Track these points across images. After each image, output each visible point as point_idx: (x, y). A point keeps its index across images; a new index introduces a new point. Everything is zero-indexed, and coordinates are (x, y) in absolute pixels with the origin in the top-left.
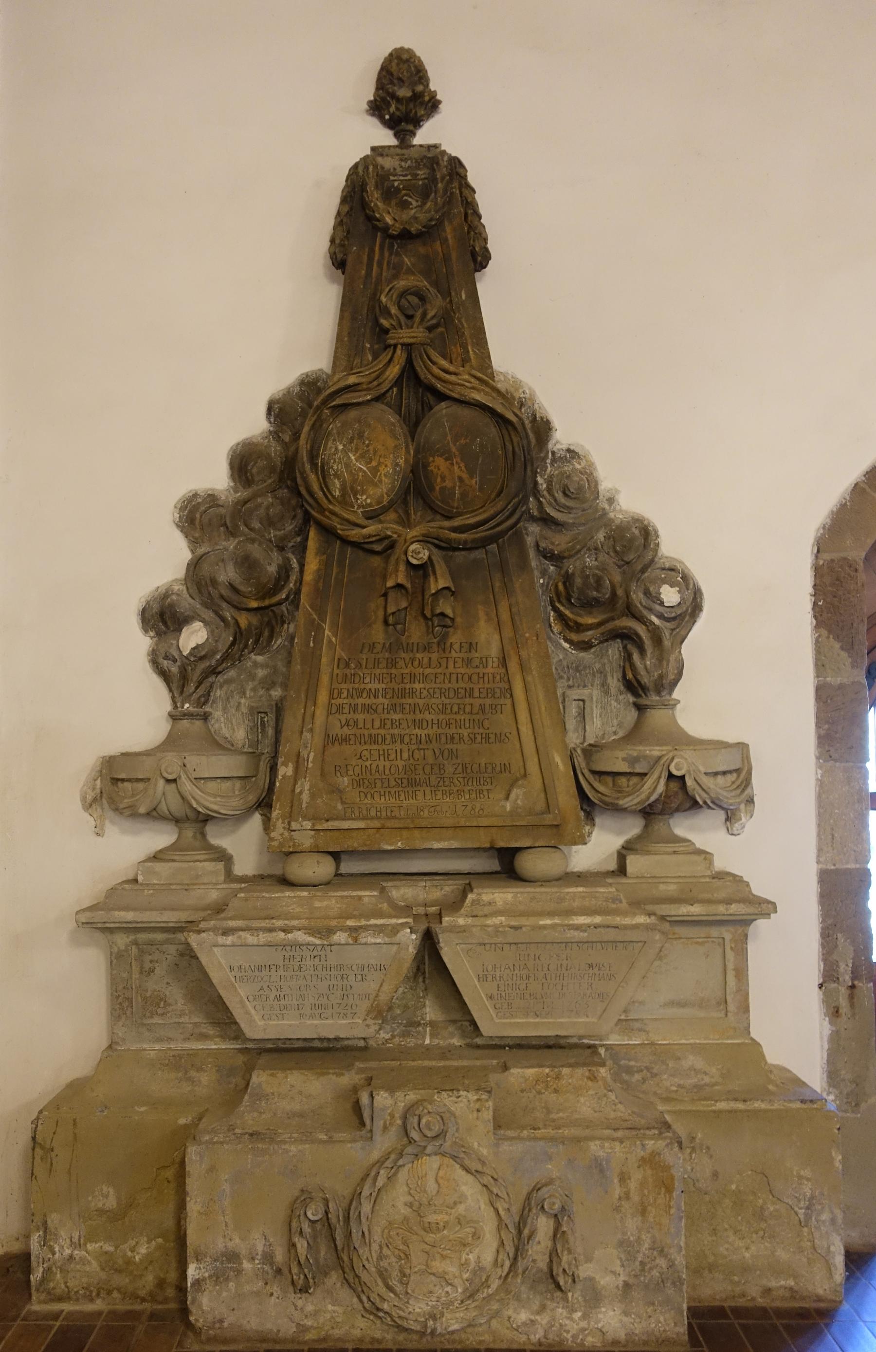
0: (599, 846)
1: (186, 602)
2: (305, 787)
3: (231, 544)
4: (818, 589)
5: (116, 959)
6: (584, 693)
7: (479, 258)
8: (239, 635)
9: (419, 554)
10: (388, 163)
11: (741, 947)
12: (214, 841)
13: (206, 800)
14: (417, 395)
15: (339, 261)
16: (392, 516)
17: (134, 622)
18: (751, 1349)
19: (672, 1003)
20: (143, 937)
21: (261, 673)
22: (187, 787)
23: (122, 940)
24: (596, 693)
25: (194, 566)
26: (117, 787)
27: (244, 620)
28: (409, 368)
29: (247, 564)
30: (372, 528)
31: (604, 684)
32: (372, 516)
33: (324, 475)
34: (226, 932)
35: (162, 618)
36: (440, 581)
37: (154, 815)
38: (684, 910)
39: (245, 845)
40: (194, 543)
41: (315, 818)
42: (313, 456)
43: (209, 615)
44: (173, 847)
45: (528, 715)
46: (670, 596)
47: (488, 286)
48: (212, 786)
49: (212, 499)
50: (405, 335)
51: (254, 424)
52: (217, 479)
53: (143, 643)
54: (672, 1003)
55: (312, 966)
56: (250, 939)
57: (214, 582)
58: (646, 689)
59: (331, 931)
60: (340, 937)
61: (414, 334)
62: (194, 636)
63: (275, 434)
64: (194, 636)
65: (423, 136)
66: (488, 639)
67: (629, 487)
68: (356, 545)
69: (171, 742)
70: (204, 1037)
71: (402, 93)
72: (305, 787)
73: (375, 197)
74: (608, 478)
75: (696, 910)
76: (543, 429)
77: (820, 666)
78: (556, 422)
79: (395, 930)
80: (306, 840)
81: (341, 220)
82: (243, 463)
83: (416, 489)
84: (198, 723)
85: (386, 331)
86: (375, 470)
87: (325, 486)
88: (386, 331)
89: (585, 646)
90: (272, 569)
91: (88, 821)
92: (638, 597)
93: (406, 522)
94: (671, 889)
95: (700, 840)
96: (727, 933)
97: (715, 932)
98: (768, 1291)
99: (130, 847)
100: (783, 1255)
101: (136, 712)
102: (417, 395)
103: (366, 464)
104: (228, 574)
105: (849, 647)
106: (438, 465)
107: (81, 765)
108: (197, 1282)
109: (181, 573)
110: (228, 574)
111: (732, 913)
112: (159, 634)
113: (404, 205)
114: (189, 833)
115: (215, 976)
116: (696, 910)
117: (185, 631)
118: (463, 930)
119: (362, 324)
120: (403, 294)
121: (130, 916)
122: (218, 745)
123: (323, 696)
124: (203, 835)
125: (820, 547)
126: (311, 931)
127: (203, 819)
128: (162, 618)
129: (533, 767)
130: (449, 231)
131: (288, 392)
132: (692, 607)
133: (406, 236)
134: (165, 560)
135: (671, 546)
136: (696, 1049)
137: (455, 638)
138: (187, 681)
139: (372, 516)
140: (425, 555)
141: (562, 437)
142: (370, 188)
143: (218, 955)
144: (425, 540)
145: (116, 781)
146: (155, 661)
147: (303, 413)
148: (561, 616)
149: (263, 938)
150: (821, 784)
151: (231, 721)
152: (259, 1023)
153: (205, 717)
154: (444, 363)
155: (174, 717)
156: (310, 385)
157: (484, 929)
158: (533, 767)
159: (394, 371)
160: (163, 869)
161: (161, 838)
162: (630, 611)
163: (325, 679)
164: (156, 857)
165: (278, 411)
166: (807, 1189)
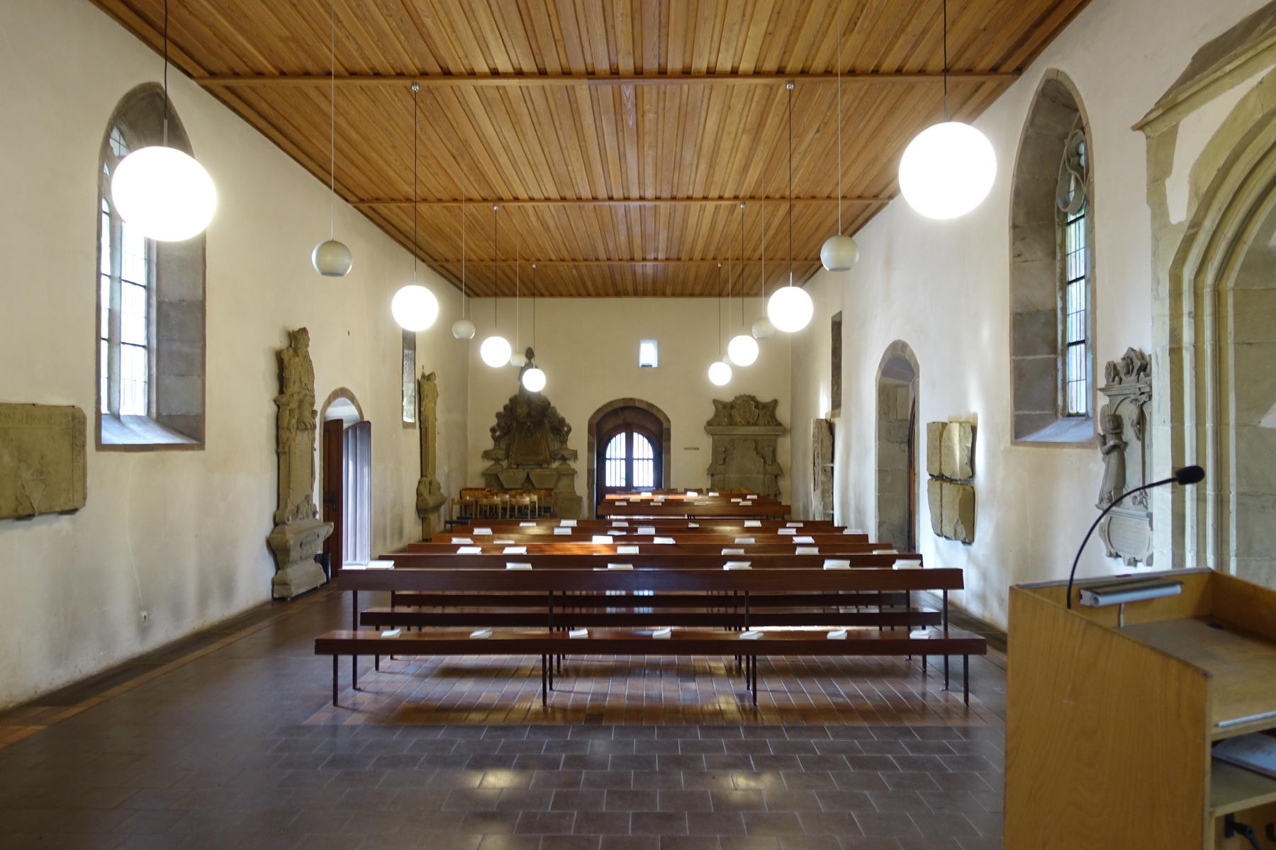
0: (555, 465)
4: (1166, 209)
18: (205, 3)
26: (486, 455)
35: (493, 430)
39: (505, 464)
45: (1250, 181)
52: (501, 410)
53: (490, 434)
58: (564, 442)
62: (498, 434)
64: (498, 434)
82: (505, 408)
99: (488, 464)
101: (489, 444)
107: (482, 451)
111: (573, 473)
132: (570, 430)
134: (494, 422)
135: (567, 421)
138: (496, 440)
143: (501, 477)
151: (503, 446)
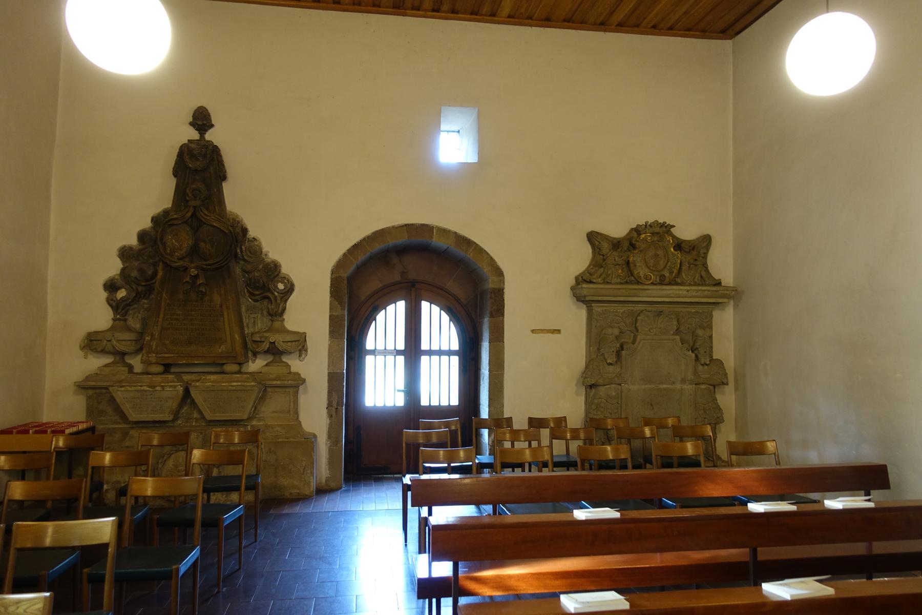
1: (120, 282)
2: (154, 344)
3: (136, 264)
5: (89, 398)
6: (255, 316)
7: (224, 178)
8: (138, 293)
9: (193, 272)
10: (193, 146)
11: (296, 394)
12: (128, 361)
13: (121, 347)
14: (196, 223)
15: (175, 174)
16: (187, 259)
17: (101, 289)
19: (274, 412)
20: (98, 391)
21: (146, 306)
22: (114, 343)
23: (91, 392)
24: (259, 316)
25: (123, 270)
27: (140, 289)
28: (194, 214)
29: (141, 270)
30: (180, 263)
31: (262, 313)
32: (180, 259)
33: (164, 244)
34: (122, 387)
36: (200, 281)
37: (103, 352)
38: (275, 382)
40: (123, 262)
41: (157, 353)
42: (162, 239)
43: (128, 286)
44: (112, 363)
46: (281, 286)
47: (226, 187)
48: (124, 343)
49: (130, 248)
50: (193, 203)
51: (147, 224)
52: (133, 241)
53: (104, 295)
54: (274, 412)
55: (150, 396)
56: (129, 388)
57: (129, 276)
58: (277, 314)
59: (155, 387)
60: (158, 388)
61: (197, 203)
62: (121, 294)
63: (153, 228)
64: (121, 294)
65: (208, 136)
66: (217, 299)
67: (273, 250)
68: (175, 268)
69: (112, 329)
70: (118, 423)
71: (202, 120)
72: (154, 344)
73: (186, 157)
74: (265, 248)
75: (278, 382)
76: (245, 231)
77: (331, 309)
78: (249, 228)
79: (175, 386)
80: (153, 360)
81: (177, 163)
83: (194, 252)
84: (122, 323)
85: (188, 201)
86: (181, 245)
87: (165, 250)
88: (188, 201)
89: (256, 301)
90: (150, 273)
91: (81, 353)
92: (271, 286)
93: (192, 262)
94: (274, 376)
95: (290, 362)
96: (291, 390)
97: (287, 390)
98: (291, 494)
99: (96, 363)
100: (295, 483)
101: (101, 317)
102: (196, 223)
103: (179, 242)
104: (135, 274)
105: (341, 303)
106: (202, 245)
107: (80, 334)
108: (107, 490)
109: (119, 272)
110: (135, 274)
111: (296, 383)
112: (110, 292)
113: (198, 160)
114: (118, 358)
115: (118, 401)
116: (278, 382)
117: (119, 292)
118: (197, 387)
119: (180, 195)
120: (194, 190)
121: (93, 383)
122: (129, 329)
123: (161, 316)
124: (123, 359)
125: (333, 272)
126: (149, 387)
127: (123, 354)
128: (111, 286)
129: (229, 339)
130: (212, 170)
131: (159, 214)
132: (290, 289)
133: (196, 170)
134: (114, 267)
135: (285, 270)
136: (278, 425)
137: (206, 298)
138: (119, 308)
139: (180, 259)
140: (196, 272)
141: (252, 233)
142: (185, 155)
143: (120, 395)
144: (196, 268)
145: (91, 340)
146: (109, 301)
147: (161, 221)
148: (248, 291)
149: (133, 388)
150: (330, 345)
151: (135, 322)
152: (134, 416)
153: (125, 320)
154: (206, 212)
155: (114, 320)
156: (166, 212)
157: (206, 385)
158: (229, 339)
159: (189, 214)
160: (107, 369)
161: (108, 360)
162: (269, 290)
163: (163, 310)
164: (106, 366)
165: (154, 220)
166: (304, 463)
